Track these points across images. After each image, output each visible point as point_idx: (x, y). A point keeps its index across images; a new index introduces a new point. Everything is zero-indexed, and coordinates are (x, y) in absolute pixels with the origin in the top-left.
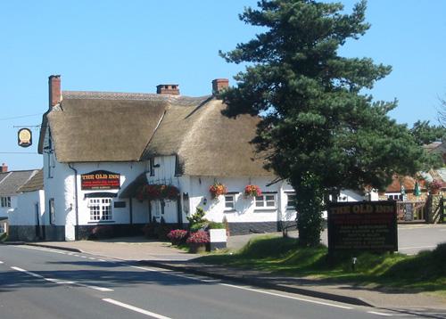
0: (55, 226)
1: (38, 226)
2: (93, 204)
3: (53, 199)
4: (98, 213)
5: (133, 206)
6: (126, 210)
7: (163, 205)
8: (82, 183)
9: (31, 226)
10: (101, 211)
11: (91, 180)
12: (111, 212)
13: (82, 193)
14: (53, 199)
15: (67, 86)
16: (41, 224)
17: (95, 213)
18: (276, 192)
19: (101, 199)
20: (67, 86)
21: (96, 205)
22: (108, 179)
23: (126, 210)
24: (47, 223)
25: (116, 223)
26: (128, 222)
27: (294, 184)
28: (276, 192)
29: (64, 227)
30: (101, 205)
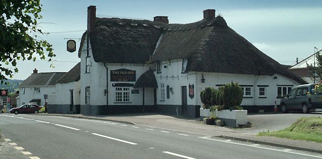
0: (91, 106)
1: (72, 105)
2: (118, 91)
3: (89, 87)
4: (121, 97)
5: (145, 96)
6: (140, 95)
7: (143, 90)
8: (111, 76)
9: (193, 105)
10: (123, 95)
11: (118, 75)
12: (129, 96)
13: (110, 83)
14: (89, 87)
15: (100, 14)
16: (74, 104)
17: (127, 96)
18: (252, 86)
19: (123, 88)
20: (100, 14)
21: (120, 91)
22: (127, 75)
23: (140, 95)
24: (83, 103)
25: (133, 104)
26: (141, 104)
27: (170, 59)
28: (252, 86)
29: (196, 106)
30: (123, 91)
